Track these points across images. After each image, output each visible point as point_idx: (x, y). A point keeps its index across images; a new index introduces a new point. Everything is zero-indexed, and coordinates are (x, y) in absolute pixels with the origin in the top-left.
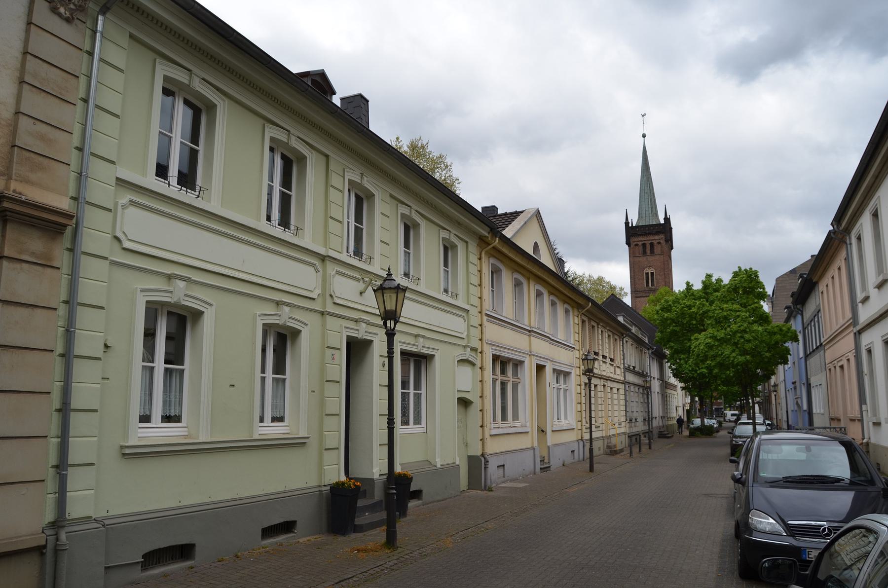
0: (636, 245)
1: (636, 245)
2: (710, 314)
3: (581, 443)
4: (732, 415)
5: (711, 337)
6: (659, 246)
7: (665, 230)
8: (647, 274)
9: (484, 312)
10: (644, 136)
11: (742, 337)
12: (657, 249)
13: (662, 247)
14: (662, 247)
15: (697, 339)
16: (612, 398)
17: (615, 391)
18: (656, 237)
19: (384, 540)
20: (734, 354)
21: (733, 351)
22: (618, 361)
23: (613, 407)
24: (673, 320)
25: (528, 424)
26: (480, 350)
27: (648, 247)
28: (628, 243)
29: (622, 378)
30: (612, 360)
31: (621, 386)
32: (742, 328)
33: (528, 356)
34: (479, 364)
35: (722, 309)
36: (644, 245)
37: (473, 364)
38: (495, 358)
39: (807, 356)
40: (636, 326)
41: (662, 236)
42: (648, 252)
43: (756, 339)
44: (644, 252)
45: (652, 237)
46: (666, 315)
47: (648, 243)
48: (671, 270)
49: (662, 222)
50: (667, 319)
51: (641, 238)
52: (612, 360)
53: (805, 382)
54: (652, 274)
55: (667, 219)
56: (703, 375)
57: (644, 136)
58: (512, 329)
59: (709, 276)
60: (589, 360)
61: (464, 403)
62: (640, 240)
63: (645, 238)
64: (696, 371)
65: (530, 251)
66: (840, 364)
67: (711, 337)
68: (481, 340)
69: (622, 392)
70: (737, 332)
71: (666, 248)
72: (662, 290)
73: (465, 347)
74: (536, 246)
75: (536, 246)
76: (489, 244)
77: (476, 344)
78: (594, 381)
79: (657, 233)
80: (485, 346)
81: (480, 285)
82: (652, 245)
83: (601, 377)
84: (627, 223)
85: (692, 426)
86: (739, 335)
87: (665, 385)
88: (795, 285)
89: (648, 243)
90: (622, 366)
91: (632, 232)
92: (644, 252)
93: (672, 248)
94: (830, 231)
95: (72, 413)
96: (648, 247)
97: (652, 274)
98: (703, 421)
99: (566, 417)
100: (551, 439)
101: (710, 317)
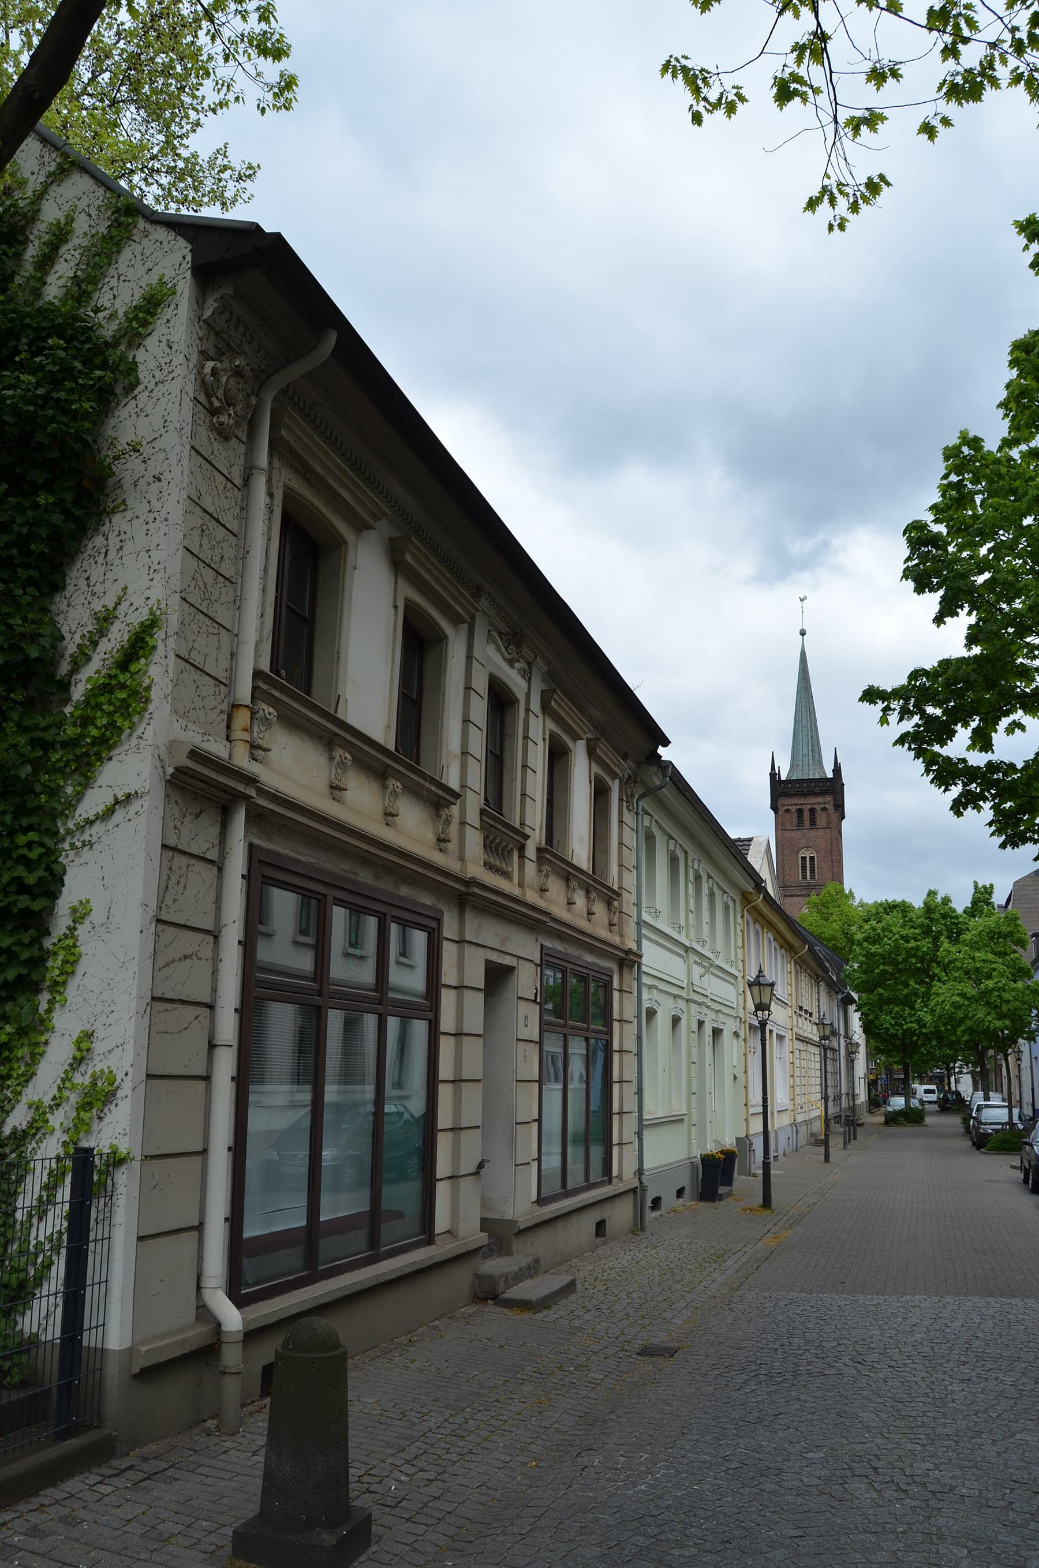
0: (788, 811)
1: (788, 811)
2: (959, 964)
4: (927, 1091)
5: (958, 995)
6: (824, 814)
7: (832, 789)
8: (804, 859)
10: (803, 633)
11: (1000, 996)
12: (821, 819)
13: (828, 815)
14: (828, 815)
15: (938, 995)
18: (820, 800)
19: (761, 1202)
20: (989, 1018)
21: (988, 1014)
24: (883, 957)
27: (807, 815)
28: (774, 807)
32: (1000, 985)
35: (973, 958)
36: (800, 812)
41: (829, 798)
43: (1016, 999)
44: (800, 823)
45: (813, 800)
46: (873, 949)
47: (806, 808)
48: (840, 855)
49: (830, 775)
50: (874, 955)
51: (794, 801)
54: (812, 859)
55: (837, 770)
56: (911, 1032)
57: (803, 633)
59: (932, 893)
62: (793, 803)
63: (802, 801)
64: (901, 1025)
67: (958, 995)
70: (993, 989)
71: (835, 817)
72: (831, 887)
73: (736, 1017)
76: (750, 903)
79: (822, 793)
82: (812, 811)
84: (774, 776)
85: (890, 1109)
86: (997, 993)
89: (806, 808)
91: (781, 790)
92: (800, 823)
93: (843, 817)
95: (440, 1085)
96: (807, 815)
97: (812, 859)
98: (907, 1102)
101: (958, 969)
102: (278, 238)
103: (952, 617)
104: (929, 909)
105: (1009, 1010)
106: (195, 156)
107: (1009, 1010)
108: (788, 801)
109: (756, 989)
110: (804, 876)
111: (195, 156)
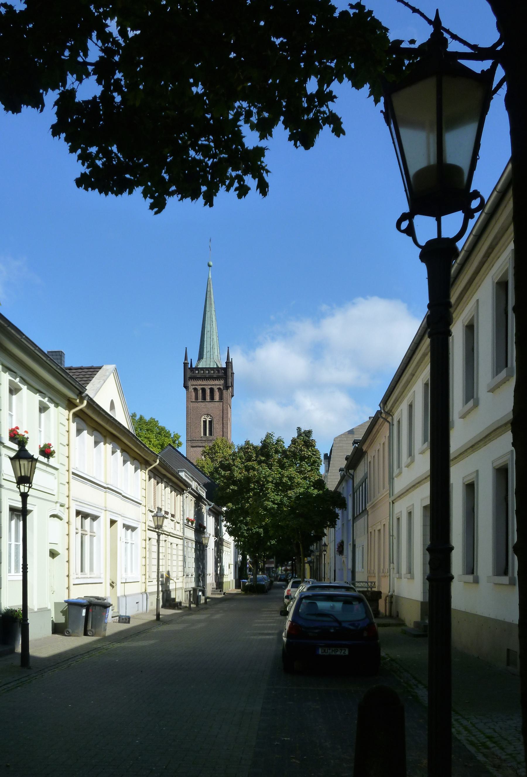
3: (145, 596)
9: (71, 470)
16: (172, 555)
17: (174, 546)
22: (178, 518)
23: (172, 563)
25: (102, 576)
26: (67, 506)
27: (208, 392)
28: (186, 387)
29: (181, 534)
30: (173, 516)
31: (180, 542)
33: (103, 511)
34: (66, 519)
36: (204, 390)
37: (61, 519)
38: (78, 513)
39: (354, 519)
40: (196, 481)
41: (222, 382)
42: (208, 398)
44: (204, 398)
47: (199, 388)
51: (200, 382)
52: (173, 516)
53: (351, 543)
58: (91, 486)
60: (159, 516)
61: (53, 554)
63: (205, 382)
65: (106, 408)
66: (379, 528)
68: (68, 496)
69: (180, 547)
73: (57, 502)
74: (112, 403)
75: (112, 403)
77: (65, 501)
78: (162, 537)
80: (72, 502)
81: (68, 445)
82: (212, 391)
83: (169, 535)
84: (185, 364)
87: (219, 544)
88: (349, 450)
90: (181, 522)
92: (204, 398)
94: (378, 411)
96: (208, 392)
97: (210, 422)
99: (132, 571)
100: (120, 590)
102: (420, 258)
103: (69, 149)
104: (265, 444)
105: (267, 489)
106: (331, 97)
107: (267, 489)
108: (195, 382)
109: (156, 518)
110: (205, 434)
111: (331, 97)
